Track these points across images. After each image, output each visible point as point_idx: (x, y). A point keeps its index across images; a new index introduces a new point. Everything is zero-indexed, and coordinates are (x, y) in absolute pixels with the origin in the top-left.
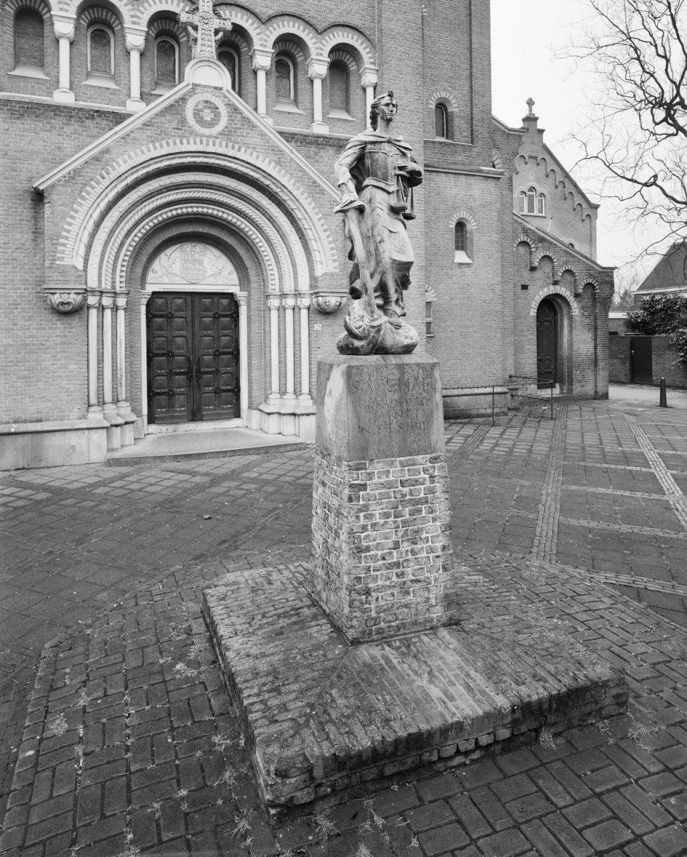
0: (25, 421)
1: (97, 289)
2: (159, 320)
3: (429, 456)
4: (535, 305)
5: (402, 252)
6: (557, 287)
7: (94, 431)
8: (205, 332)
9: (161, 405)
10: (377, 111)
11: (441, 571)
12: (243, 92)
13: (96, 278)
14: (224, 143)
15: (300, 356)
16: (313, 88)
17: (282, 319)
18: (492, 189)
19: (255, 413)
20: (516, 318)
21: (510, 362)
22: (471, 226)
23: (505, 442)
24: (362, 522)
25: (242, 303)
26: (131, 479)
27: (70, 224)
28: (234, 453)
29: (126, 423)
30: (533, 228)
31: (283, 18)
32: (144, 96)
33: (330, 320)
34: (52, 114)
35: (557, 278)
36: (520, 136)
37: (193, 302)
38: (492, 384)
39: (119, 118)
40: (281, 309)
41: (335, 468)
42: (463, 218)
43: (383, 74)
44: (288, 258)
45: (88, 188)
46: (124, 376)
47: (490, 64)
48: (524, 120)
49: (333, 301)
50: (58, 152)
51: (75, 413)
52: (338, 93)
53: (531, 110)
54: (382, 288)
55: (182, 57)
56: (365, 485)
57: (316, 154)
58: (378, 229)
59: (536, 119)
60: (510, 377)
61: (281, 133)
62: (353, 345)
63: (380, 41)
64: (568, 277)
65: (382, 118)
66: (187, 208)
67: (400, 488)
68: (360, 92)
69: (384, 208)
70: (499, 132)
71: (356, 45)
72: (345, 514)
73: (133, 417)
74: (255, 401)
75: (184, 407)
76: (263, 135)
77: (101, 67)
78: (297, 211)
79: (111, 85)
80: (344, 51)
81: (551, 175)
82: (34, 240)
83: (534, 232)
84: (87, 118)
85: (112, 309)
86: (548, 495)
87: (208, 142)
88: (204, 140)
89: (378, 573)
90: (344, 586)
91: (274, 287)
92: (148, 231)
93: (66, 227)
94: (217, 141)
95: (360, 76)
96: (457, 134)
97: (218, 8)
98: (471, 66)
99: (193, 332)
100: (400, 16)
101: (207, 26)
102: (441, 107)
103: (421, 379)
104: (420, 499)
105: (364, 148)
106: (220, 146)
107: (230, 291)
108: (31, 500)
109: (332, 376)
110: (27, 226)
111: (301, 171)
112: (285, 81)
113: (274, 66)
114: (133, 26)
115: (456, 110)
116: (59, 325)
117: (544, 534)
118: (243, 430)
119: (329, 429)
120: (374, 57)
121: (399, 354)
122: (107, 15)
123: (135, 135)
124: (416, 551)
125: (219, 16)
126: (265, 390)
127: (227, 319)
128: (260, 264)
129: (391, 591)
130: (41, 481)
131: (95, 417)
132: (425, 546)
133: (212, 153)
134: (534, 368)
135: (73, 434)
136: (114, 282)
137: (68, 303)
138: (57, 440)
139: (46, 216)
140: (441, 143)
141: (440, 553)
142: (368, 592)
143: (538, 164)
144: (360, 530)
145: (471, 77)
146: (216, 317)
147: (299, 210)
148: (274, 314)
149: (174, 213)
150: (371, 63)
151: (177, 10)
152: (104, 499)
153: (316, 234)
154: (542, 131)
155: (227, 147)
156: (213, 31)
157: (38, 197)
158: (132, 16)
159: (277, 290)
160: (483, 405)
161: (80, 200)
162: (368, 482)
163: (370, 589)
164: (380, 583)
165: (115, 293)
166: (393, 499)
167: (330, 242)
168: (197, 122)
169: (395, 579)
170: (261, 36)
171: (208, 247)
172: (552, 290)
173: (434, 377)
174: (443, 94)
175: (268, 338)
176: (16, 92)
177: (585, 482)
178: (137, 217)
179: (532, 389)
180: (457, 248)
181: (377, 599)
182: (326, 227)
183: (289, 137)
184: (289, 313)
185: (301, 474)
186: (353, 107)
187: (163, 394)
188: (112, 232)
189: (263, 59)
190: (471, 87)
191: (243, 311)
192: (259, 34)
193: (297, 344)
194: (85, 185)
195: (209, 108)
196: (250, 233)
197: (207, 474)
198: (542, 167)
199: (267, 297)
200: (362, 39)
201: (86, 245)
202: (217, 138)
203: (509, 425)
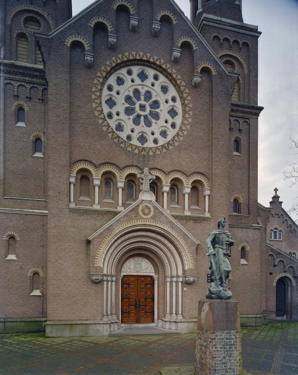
0: (83, 320)
2: (125, 285)
3: (235, 331)
4: (275, 281)
5: (227, 267)
6: (286, 274)
8: (142, 290)
9: (126, 317)
13: (106, 271)
14: (152, 221)
19: (160, 321)
22: (248, 249)
24: (214, 349)
27: (99, 252)
28: (154, 335)
29: (115, 322)
30: (275, 249)
32: (123, 205)
33: (190, 286)
35: (286, 270)
39: (116, 214)
40: (171, 282)
42: (244, 246)
43: (212, 191)
46: (114, 305)
47: (257, 182)
48: (273, 198)
51: (99, 318)
53: (276, 193)
54: (221, 279)
56: (215, 338)
60: (264, 311)
61: (173, 216)
63: (212, 178)
64: (291, 269)
65: (222, 226)
68: (203, 198)
69: (222, 254)
73: (117, 321)
76: (166, 217)
79: (112, 201)
82: (86, 257)
83: (275, 250)
84: (104, 214)
87: (146, 221)
88: (145, 220)
89: (219, 365)
91: (168, 273)
93: (98, 253)
94: (150, 221)
97: (150, 170)
98: (249, 183)
102: (236, 200)
104: (232, 344)
105: (215, 236)
106: (151, 222)
107: (151, 275)
108: (88, 346)
109: (204, 306)
111: (180, 230)
112: (174, 195)
113: (170, 190)
114: (120, 180)
115: (242, 201)
116: (94, 287)
120: (209, 184)
121: (226, 299)
123: (122, 219)
124: (231, 359)
125: (151, 174)
127: (150, 285)
131: (105, 319)
132: (233, 358)
133: (148, 225)
134: (275, 308)
135: (98, 325)
136: (112, 272)
137: (98, 279)
139: (91, 249)
140: (236, 215)
141: (238, 361)
142: (215, 370)
146: (146, 284)
147: (179, 245)
148: (168, 284)
150: (208, 187)
157: (89, 242)
158: (120, 176)
159: (170, 275)
160: (252, 322)
161: (102, 243)
162: (216, 338)
163: (216, 369)
165: (112, 276)
168: (143, 214)
169: (224, 367)
172: (283, 275)
174: (237, 195)
176: (80, 206)
177: (294, 352)
178: (120, 248)
179: (274, 316)
180: (242, 258)
181: (218, 373)
183: (176, 217)
184: (174, 284)
185: (180, 343)
188: (112, 254)
190: (249, 192)
191: (156, 282)
192: (165, 179)
194: (104, 238)
195: (147, 208)
196: (157, 251)
197: (146, 341)
198: (281, 219)
199: (166, 277)
201: (104, 260)
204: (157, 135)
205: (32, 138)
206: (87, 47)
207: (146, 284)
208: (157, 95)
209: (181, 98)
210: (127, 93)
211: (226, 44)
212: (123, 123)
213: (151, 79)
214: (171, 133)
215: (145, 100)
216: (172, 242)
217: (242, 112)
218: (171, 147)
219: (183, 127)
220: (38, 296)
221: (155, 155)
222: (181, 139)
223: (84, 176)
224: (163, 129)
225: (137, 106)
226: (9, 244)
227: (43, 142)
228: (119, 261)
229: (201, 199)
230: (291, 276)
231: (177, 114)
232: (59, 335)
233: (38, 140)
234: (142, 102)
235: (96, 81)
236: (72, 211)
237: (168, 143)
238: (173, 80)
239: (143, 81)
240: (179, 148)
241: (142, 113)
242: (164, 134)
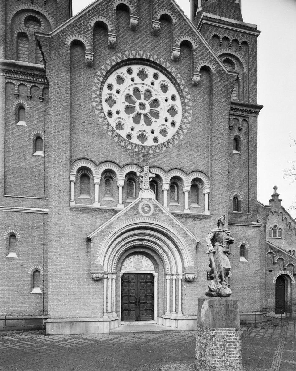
1: (107, 272)
2: (126, 283)
5: (227, 265)
6: (285, 271)
7: (105, 322)
8: (142, 288)
10: (220, 222)
11: (238, 364)
12: (158, 199)
13: (106, 269)
14: (152, 219)
15: (178, 298)
16: (184, 196)
18: (257, 231)
19: (160, 319)
20: (267, 284)
21: (263, 302)
22: (247, 246)
23: (261, 334)
24: (214, 346)
25: (155, 277)
26: (120, 339)
27: (99, 250)
28: (154, 332)
29: (116, 320)
30: (274, 246)
31: (174, 170)
32: (123, 203)
33: (190, 284)
34: (93, 211)
35: (285, 267)
36: (270, 208)
37: (138, 276)
38: (255, 311)
39: (116, 212)
40: (171, 280)
41: (205, 331)
44: (174, 261)
45: (105, 237)
46: (114, 303)
47: (257, 180)
49: (191, 277)
50: (95, 224)
52: (194, 196)
53: (275, 191)
54: (220, 276)
55: (137, 187)
56: (215, 336)
57: (186, 221)
58: (220, 258)
59: (278, 195)
61: (172, 214)
62: (211, 293)
65: (221, 224)
66: (139, 242)
67: (226, 337)
68: (203, 196)
70: (259, 207)
71: (202, 178)
72: (208, 344)
73: (118, 318)
74: (160, 314)
75: (134, 315)
76: (166, 215)
77: (107, 193)
78: (178, 243)
79: (112, 199)
80: (197, 180)
81: (285, 220)
82: (87, 255)
85: (111, 279)
86: (277, 352)
87: (146, 219)
90: (208, 366)
91: (168, 271)
92: (123, 251)
93: (98, 251)
94: (150, 218)
95: (203, 190)
96: (242, 209)
97: (150, 169)
98: (249, 181)
99: (137, 287)
100: (219, 166)
101: (146, 176)
102: (236, 198)
103: (233, 305)
104: (232, 341)
110: (85, 250)
111: (180, 228)
116: (94, 285)
117: (275, 364)
118: (156, 325)
119: (203, 319)
122: (111, 175)
125: (151, 172)
126: (164, 310)
128: (163, 263)
129: (222, 368)
130: (91, 338)
131: (106, 317)
132: (233, 356)
133: (148, 223)
135: (99, 323)
137: (98, 277)
139: (91, 247)
140: (235, 213)
141: (238, 358)
142: (215, 368)
143: (279, 215)
144: (213, 349)
145: (248, 186)
146: (146, 282)
147: (179, 243)
148: (168, 282)
149: (133, 244)
150: (207, 185)
151: (136, 171)
152: (113, 345)
153: (185, 252)
154: (281, 200)
155: (153, 220)
156: (149, 178)
157: (89, 240)
160: (252, 320)
162: (216, 335)
163: (216, 367)
164: (219, 365)
165: (112, 273)
166: (223, 341)
167: (191, 255)
169: (223, 365)
170: (165, 178)
171: (143, 256)
172: (283, 272)
173: (237, 304)
174: (236, 194)
175: (166, 290)
178: (120, 246)
179: (273, 314)
180: (241, 256)
182: (189, 249)
183: (176, 215)
184: (174, 281)
186: (200, 202)
187: (127, 310)
189: (166, 186)
190: (248, 190)
192: (165, 177)
193: (177, 293)
195: (147, 206)
197: (146, 339)
198: (280, 217)
199: (166, 275)
200: (202, 174)
201: (104, 257)
202: (150, 217)
203: (262, 328)
204: (157, 134)
205: (32, 137)
207: (146, 282)
208: (157, 93)
209: (181, 96)
210: (127, 92)
211: (225, 43)
212: (123, 122)
213: (150, 78)
214: (171, 131)
216: (172, 240)
217: (242, 111)
218: (171, 146)
219: (183, 126)
222: (181, 137)
224: (163, 127)
225: (137, 105)
226: (10, 242)
228: (119, 259)
229: (201, 197)
230: (290, 274)
232: (60, 332)
233: (38, 138)
234: (142, 101)
235: (96, 80)
236: (72, 209)
237: (168, 142)
238: (172, 79)
239: (142, 80)
240: (179, 147)
241: (142, 112)
242: (164, 132)
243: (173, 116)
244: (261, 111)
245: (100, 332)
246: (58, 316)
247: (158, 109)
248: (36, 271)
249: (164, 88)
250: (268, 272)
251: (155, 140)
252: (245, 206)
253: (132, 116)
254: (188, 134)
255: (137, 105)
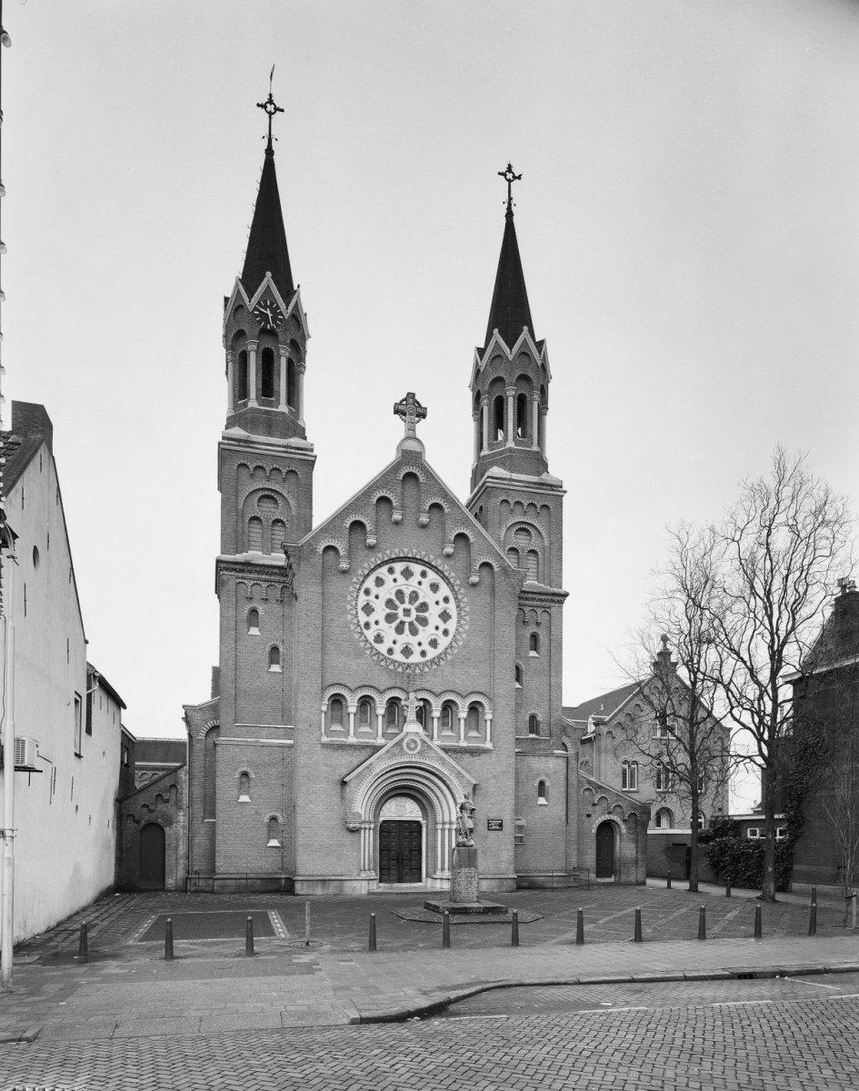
4: (595, 826)
6: (611, 816)
17: (443, 834)
19: (430, 880)
40: (443, 830)
53: (665, 646)
71: (484, 703)
91: (439, 819)
102: (533, 717)
131: (363, 875)
134: (594, 864)
138: (347, 884)
146: (411, 832)
148: (439, 832)
172: (607, 817)
174: (533, 711)
180: (540, 795)
184: (447, 831)
186: (480, 730)
189: (436, 713)
191: (424, 829)
199: (436, 824)
201: (361, 803)
204: (426, 646)
205: (268, 649)
206: (342, 553)
207: (411, 832)
208: (426, 595)
209: (456, 598)
210: (388, 596)
211: (518, 508)
212: (383, 634)
213: (417, 577)
214: (444, 642)
215: (410, 603)
216: (444, 782)
218: (442, 663)
219: (458, 637)
220: (277, 847)
221: (422, 674)
222: (455, 651)
223: (337, 701)
224: (433, 637)
225: (400, 612)
226: (241, 783)
227: (281, 654)
229: (481, 724)
231: (450, 617)
232: (310, 893)
233: (275, 649)
234: (407, 606)
236: (325, 746)
237: (439, 657)
238: (444, 578)
239: (407, 579)
240: (453, 663)
241: (407, 619)
242: (434, 643)
243: (445, 621)
244: (568, 598)
245: (356, 893)
246: (308, 873)
247: (426, 614)
248: (274, 819)
249: (434, 587)
250: (585, 818)
251: (423, 654)
252: (546, 728)
253: (388, 611)
254: (465, 646)
255: (400, 612)
